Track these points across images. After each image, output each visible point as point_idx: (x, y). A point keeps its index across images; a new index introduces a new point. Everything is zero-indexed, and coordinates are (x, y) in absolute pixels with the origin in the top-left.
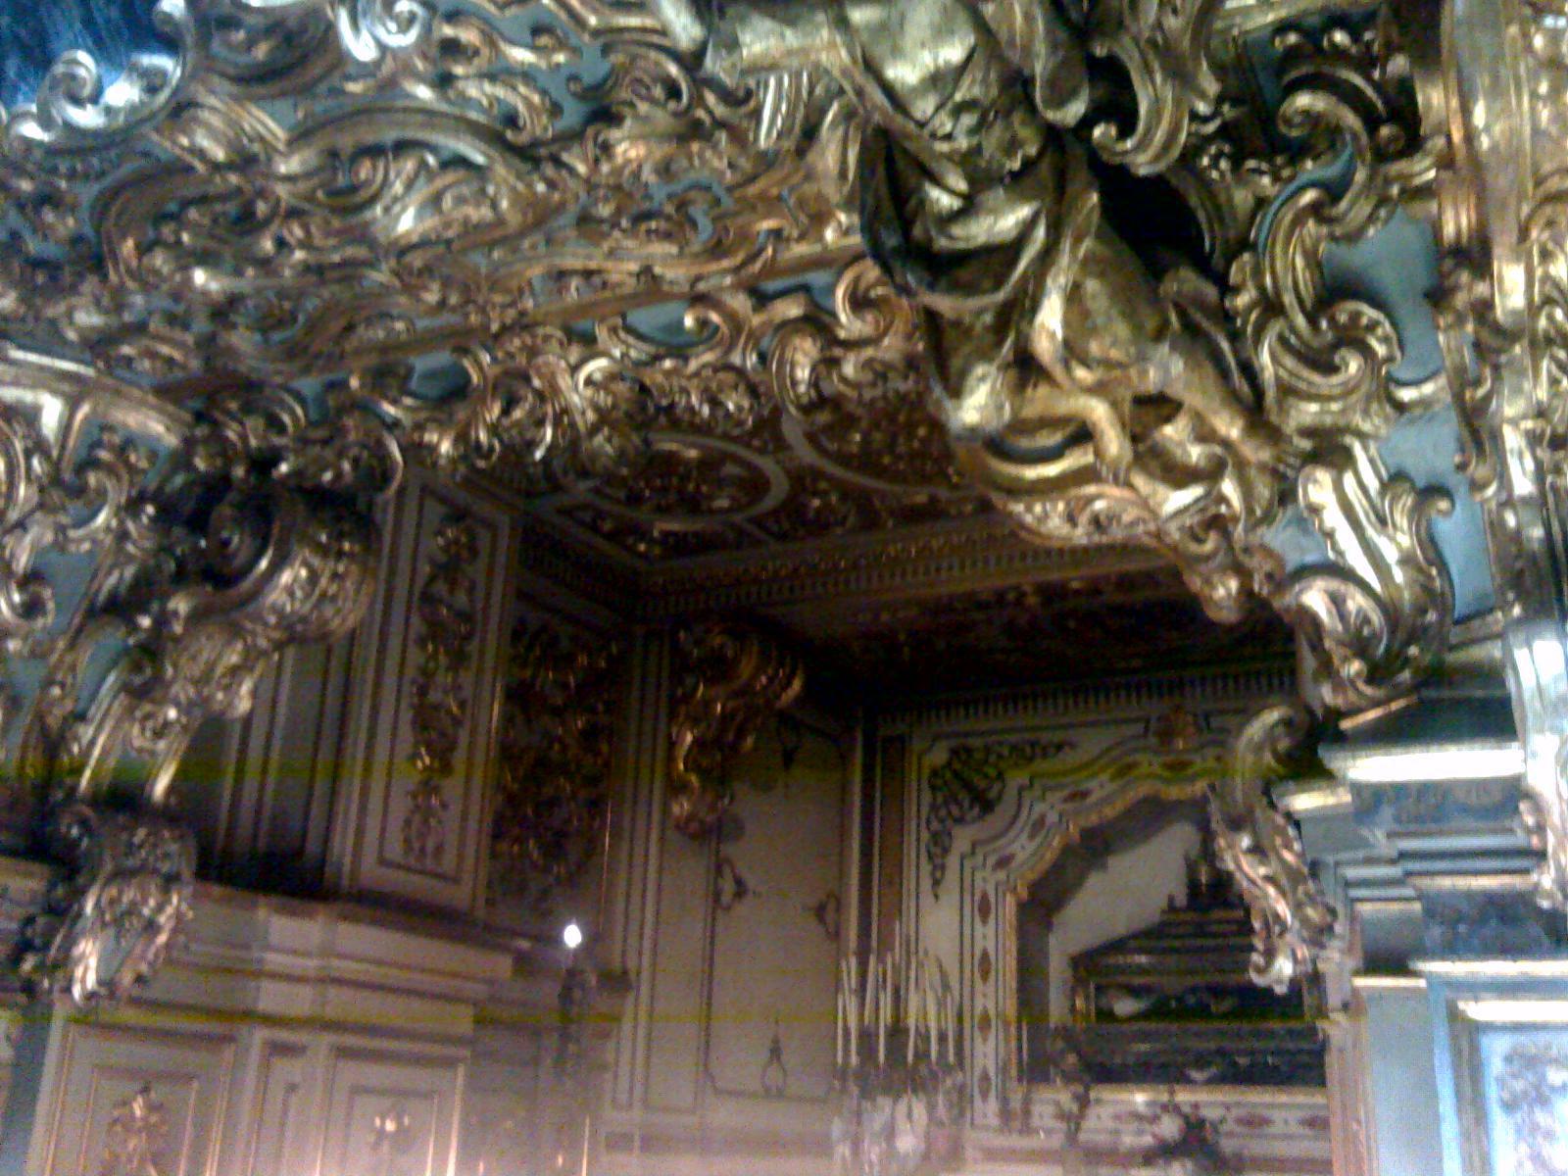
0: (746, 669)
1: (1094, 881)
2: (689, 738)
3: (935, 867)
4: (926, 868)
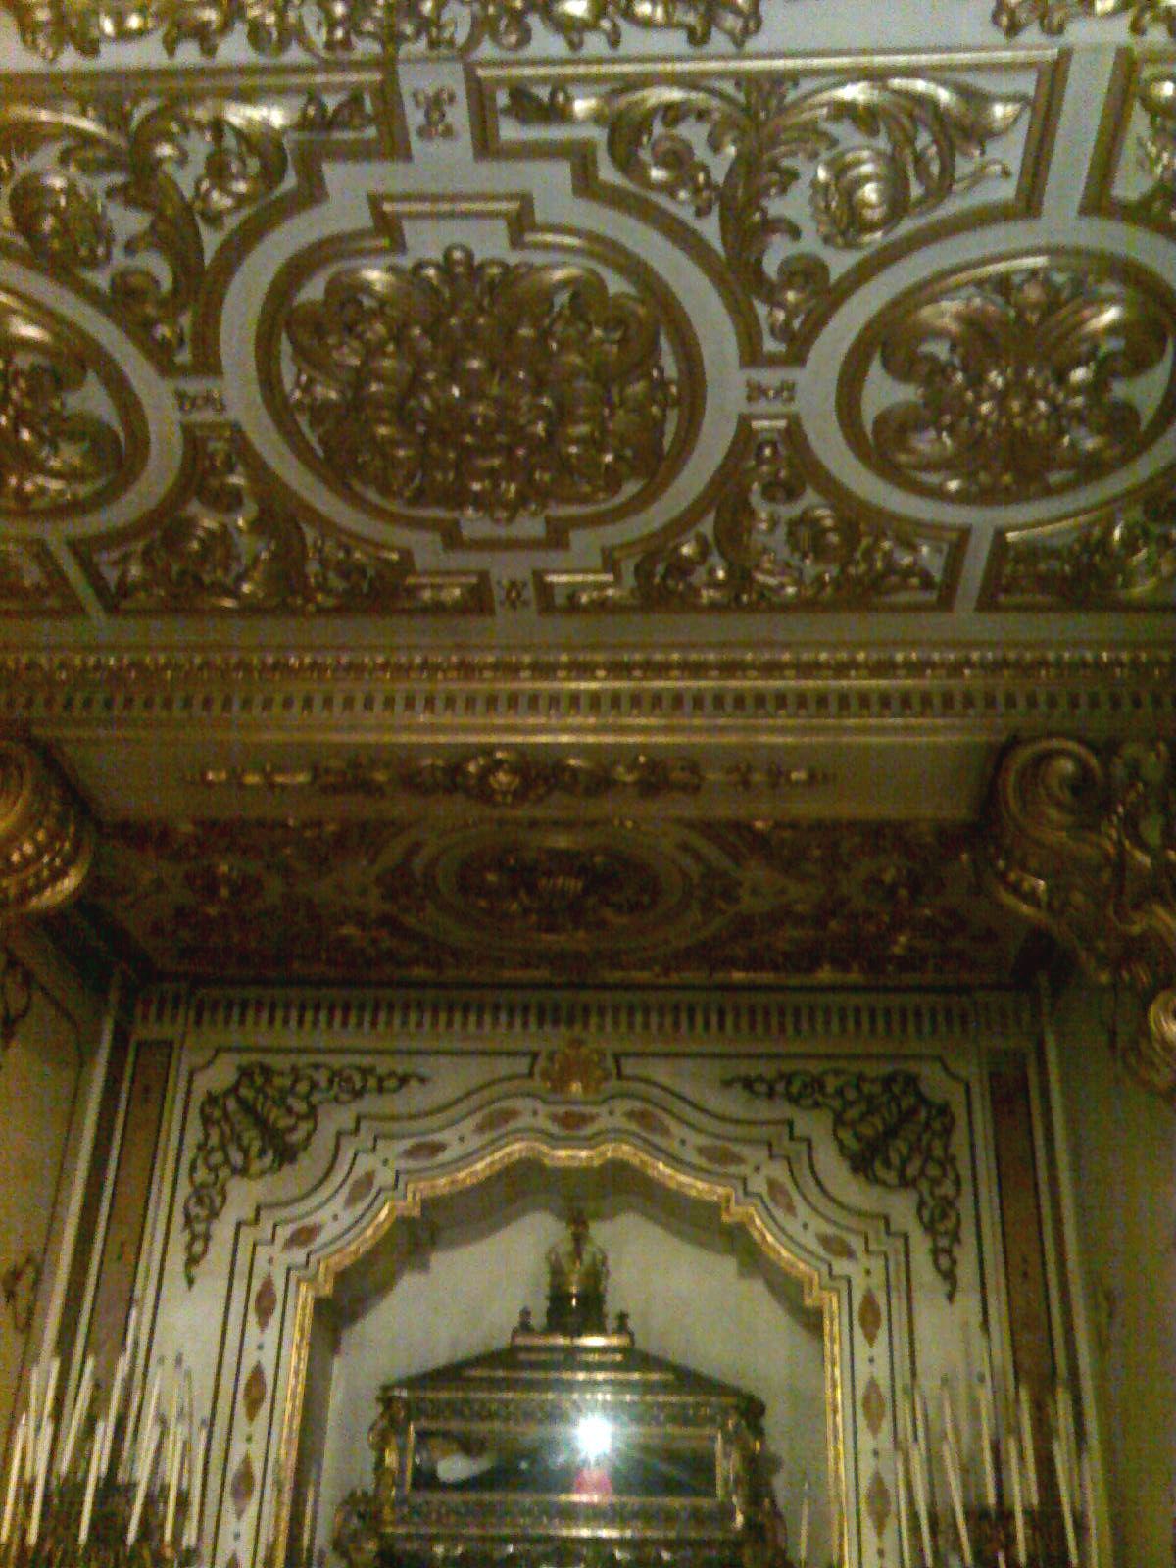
1: (409, 1283)
4: (179, 1238)
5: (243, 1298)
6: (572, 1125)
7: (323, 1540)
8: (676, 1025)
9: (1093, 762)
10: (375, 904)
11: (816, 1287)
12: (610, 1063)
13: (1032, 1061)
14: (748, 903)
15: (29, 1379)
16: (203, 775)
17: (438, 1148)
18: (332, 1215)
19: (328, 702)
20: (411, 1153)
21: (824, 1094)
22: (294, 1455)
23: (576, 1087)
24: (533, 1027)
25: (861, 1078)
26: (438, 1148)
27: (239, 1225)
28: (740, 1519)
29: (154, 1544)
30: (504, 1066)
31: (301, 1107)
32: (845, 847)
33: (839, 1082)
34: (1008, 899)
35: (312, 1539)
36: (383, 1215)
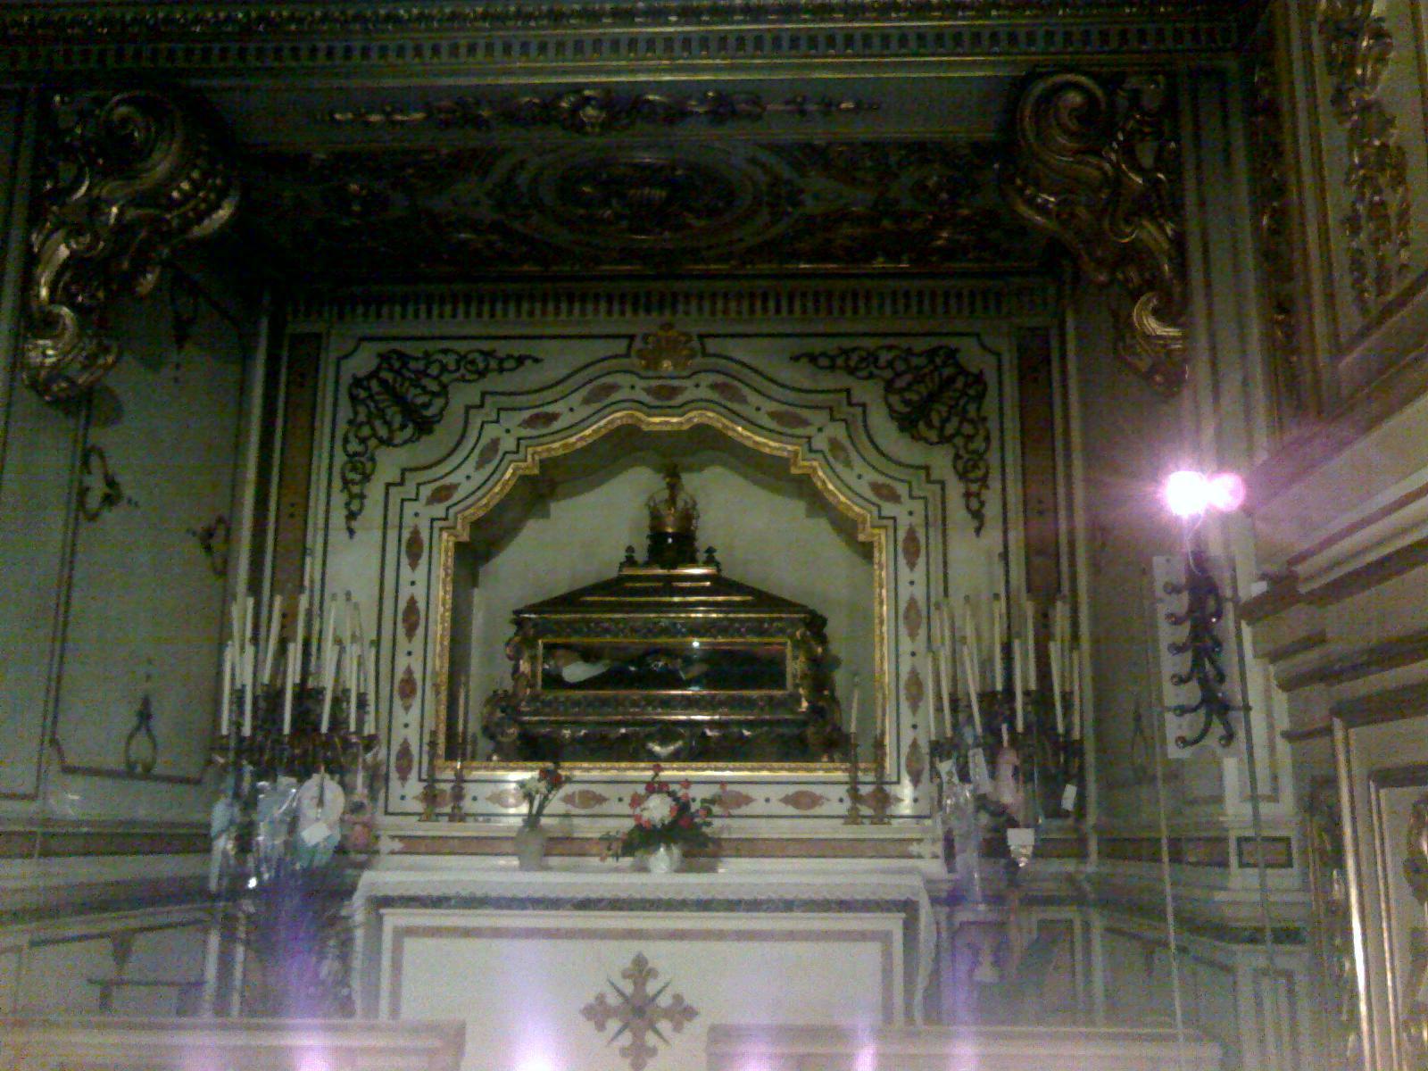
0: (161, 165)
1: (532, 530)
2: (64, 252)
3: (352, 497)
4: (339, 498)
5: (396, 542)
6: (665, 397)
7: (474, 727)
8: (752, 311)
9: (1099, 93)
10: (486, 212)
11: (868, 524)
12: (695, 343)
13: (1054, 332)
14: (811, 206)
15: (230, 613)
16: (331, 115)
17: (553, 417)
18: (466, 476)
19: (436, 50)
20: (531, 422)
21: (877, 367)
22: (447, 665)
23: (667, 364)
24: (629, 314)
25: (909, 351)
26: (553, 417)
27: (388, 485)
28: (805, 704)
29: (342, 732)
30: (601, 348)
31: (434, 387)
32: (893, 160)
33: (891, 355)
34: (1023, 209)
35: (465, 727)
36: (508, 475)
